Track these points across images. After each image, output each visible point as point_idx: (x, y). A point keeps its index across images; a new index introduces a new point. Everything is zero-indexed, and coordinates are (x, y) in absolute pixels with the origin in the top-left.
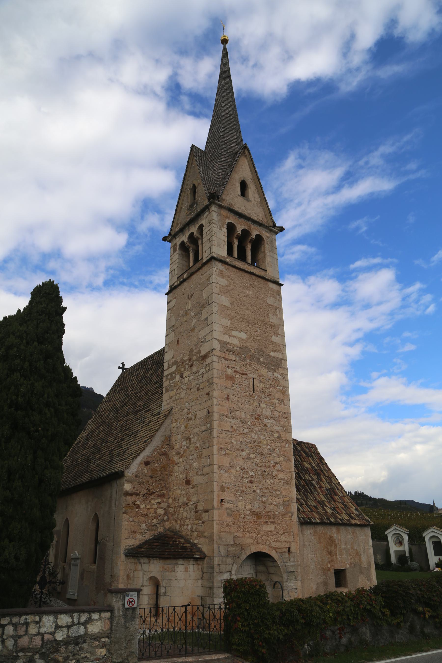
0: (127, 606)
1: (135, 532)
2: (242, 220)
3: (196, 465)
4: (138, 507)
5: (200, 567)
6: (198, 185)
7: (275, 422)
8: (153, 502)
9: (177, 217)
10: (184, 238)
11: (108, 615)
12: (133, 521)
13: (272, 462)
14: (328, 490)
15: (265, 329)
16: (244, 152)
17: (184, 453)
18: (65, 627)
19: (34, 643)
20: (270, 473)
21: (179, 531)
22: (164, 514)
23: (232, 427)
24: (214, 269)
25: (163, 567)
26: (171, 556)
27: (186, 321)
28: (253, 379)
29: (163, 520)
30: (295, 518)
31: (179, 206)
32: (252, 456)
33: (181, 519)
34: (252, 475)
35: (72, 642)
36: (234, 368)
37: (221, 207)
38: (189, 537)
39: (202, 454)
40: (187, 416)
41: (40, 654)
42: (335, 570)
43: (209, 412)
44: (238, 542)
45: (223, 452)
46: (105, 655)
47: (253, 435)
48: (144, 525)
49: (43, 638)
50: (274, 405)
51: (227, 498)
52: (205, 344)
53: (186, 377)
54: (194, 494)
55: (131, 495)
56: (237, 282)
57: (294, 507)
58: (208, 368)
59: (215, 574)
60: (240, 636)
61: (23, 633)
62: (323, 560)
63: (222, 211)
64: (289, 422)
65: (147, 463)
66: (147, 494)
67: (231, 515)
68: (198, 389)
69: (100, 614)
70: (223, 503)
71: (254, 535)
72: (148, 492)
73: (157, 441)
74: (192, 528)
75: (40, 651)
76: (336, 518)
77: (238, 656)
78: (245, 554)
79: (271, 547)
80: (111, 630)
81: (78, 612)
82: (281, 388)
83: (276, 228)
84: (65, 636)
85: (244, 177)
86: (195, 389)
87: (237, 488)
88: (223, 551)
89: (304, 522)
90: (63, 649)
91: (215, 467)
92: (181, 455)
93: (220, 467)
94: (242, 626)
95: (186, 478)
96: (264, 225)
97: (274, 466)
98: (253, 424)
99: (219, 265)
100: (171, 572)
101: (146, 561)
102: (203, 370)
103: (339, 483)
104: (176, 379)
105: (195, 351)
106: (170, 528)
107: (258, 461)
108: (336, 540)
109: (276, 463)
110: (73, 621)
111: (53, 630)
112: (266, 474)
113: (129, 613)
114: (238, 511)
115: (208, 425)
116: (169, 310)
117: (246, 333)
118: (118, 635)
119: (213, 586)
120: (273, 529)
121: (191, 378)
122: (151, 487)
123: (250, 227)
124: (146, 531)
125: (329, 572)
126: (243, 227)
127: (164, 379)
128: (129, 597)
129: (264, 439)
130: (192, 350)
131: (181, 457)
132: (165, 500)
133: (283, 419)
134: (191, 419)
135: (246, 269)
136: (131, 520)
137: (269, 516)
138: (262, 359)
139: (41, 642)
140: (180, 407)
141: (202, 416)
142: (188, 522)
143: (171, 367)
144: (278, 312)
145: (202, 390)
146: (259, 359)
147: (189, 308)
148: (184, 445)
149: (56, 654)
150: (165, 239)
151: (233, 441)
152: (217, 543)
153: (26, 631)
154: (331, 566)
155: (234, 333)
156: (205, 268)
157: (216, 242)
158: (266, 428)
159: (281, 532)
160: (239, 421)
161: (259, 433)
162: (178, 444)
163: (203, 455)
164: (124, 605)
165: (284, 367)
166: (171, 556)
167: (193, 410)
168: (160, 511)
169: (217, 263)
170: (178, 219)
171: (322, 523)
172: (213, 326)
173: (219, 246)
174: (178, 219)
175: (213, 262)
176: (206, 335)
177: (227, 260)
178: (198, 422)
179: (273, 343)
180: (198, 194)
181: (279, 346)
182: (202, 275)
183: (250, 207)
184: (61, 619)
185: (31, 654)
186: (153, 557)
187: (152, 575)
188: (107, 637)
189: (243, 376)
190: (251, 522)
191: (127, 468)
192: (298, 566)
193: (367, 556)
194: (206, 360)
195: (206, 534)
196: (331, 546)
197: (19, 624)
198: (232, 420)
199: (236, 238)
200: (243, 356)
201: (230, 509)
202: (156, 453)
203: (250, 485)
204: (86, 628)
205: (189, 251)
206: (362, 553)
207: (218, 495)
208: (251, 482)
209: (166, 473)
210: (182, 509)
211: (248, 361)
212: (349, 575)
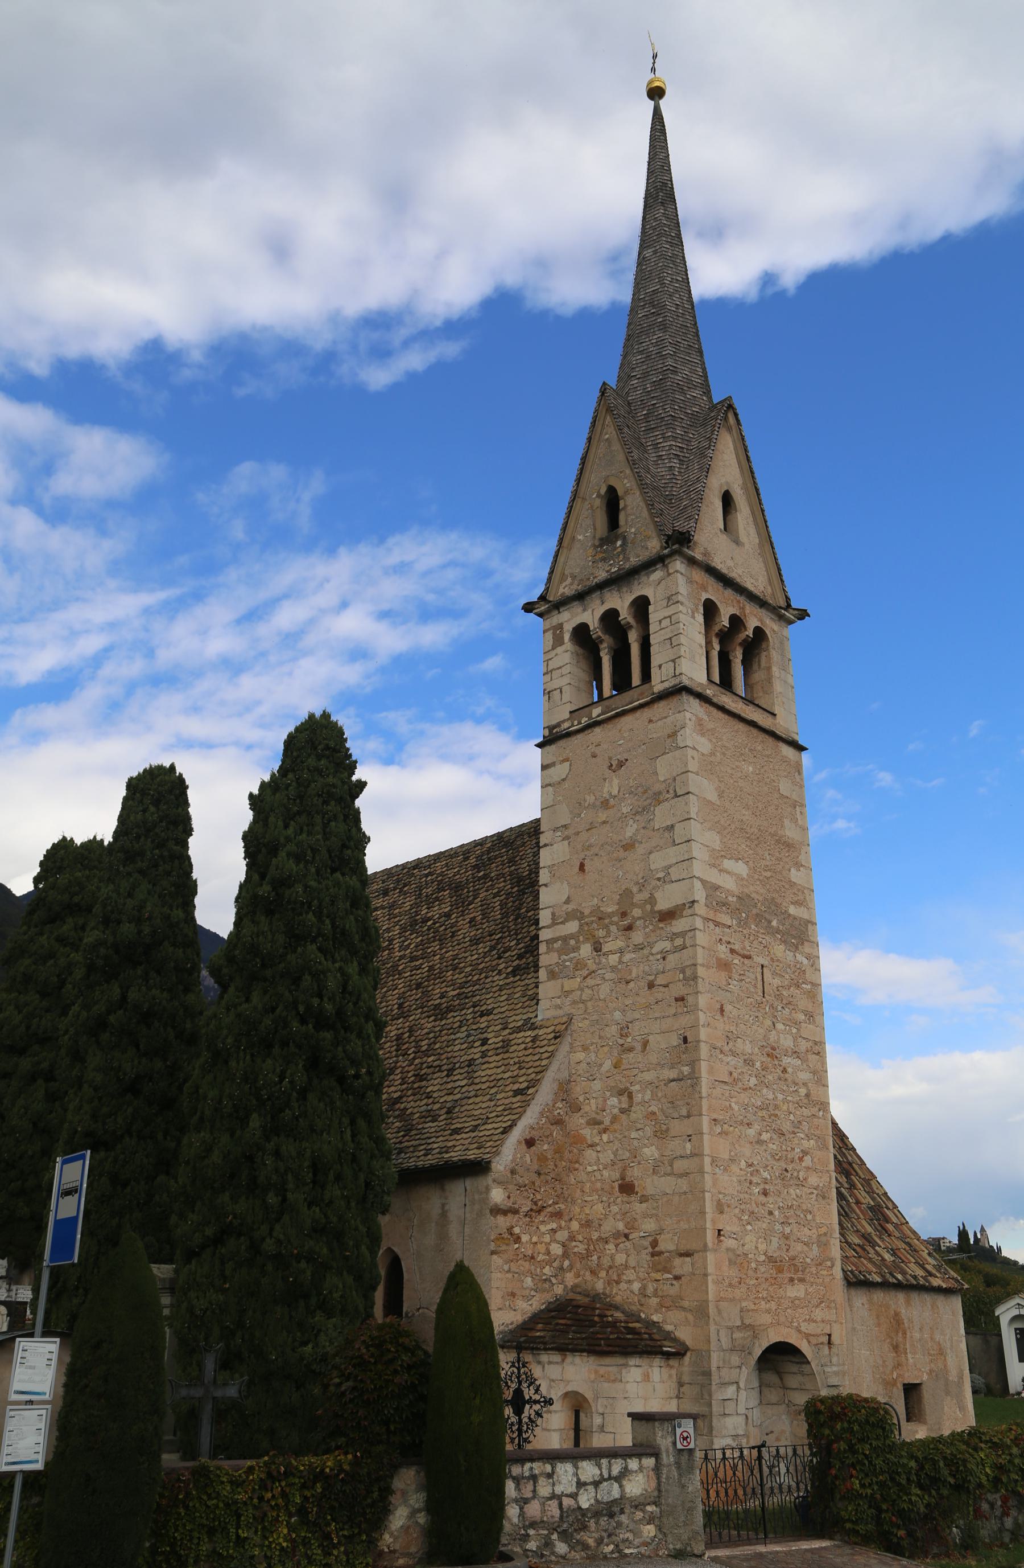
0: (679, 1446)
1: (513, 1295)
2: (729, 592)
3: (650, 1152)
4: (518, 1240)
5: (674, 1372)
6: (627, 492)
7: (800, 1062)
8: (543, 1228)
9: (561, 559)
10: (591, 615)
11: (649, 1462)
12: (509, 1271)
13: (797, 1150)
14: (871, 1208)
15: (777, 854)
16: (726, 419)
17: (612, 1123)
18: (591, 1483)
19: (549, 1513)
20: (795, 1174)
21: (604, 1294)
22: (563, 1255)
23: (731, 1074)
24: (688, 715)
25: (596, 1372)
26: (617, 1349)
27: (604, 822)
28: (762, 966)
29: (561, 1268)
30: (838, 1274)
31: (569, 531)
32: (765, 1136)
33: (610, 1267)
34: (766, 1179)
35: (605, 1512)
36: (729, 943)
37: (692, 561)
38: (633, 1308)
39: (668, 1130)
40: (621, 1041)
41: (559, 1533)
42: (904, 1385)
43: (685, 1040)
44: (747, 1322)
45: (718, 1130)
46: (655, 1536)
47: (765, 1091)
48: (529, 1279)
49: (560, 1505)
50: (797, 1023)
51: (728, 1228)
52: (667, 886)
53: (612, 952)
54: (645, 1216)
55: (505, 1212)
56: (727, 745)
57: (835, 1251)
58: (679, 942)
59: (714, 1387)
60: (859, 1504)
61: (530, 1495)
62: (884, 1362)
63: (694, 572)
64: (824, 1063)
65: (530, 1143)
66: (531, 1210)
67: (735, 1263)
68: (651, 985)
69: (640, 1460)
70: (722, 1238)
71: (773, 1305)
72: (534, 1207)
73: (545, 1094)
74: (644, 1288)
75: (558, 1526)
76: (904, 1273)
77: (856, 1544)
78: (760, 1345)
79: (800, 1331)
80: (659, 1491)
81: (607, 1457)
82: (809, 987)
83: (791, 611)
84: (593, 1501)
85: (727, 483)
86: (643, 984)
87: (743, 1207)
88: (725, 1342)
89: (856, 1282)
90: (592, 1524)
91: (707, 1160)
92: (602, 1126)
93: (714, 1161)
94: (863, 1486)
95: (623, 1178)
96: (770, 605)
97: (801, 1159)
98: (765, 1068)
99: (695, 703)
100: (614, 1381)
101: (556, 1357)
102: (666, 945)
103: (886, 1193)
104: (581, 952)
105: (639, 898)
106: (575, 1286)
107: (774, 1147)
108: (905, 1321)
109: (805, 1153)
110: (601, 1474)
111: (574, 1489)
112: (789, 1175)
113: (685, 1457)
114: (746, 1255)
115: (686, 1070)
116: (547, 785)
117: (747, 863)
118: (670, 1501)
119: (711, 1413)
120: (801, 1294)
121: (627, 957)
122: (539, 1197)
123: (743, 608)
124: (533, 1293)
125: (895, 1389)
126: (732, 611)
127: (543, 948)
128: (682, 1430)
129: (784, 1101)
130: (627, 894)
131: (605, 1131)
132: (563, 1223)
133: (814, 1056)
134: (631, 1050)
135: (743, 715)
136: (506, 1267)
137: (795, 1265)
138: (774, 923)
139: (559, 1512)
140: (595, 1017)
141: (663, 1046)
142: (630, 1274)
143: (562, 923)
144: (798, 813)
145: (662, 989)
146: (770, 922)
147: (615, 792)
148: (613, 1106)
149: (582, 1533)
150: (528, 608)
151: (733, 1104)
152: (716, 1324)
153: (534, 1491)
154: (899, 1376)
155: (728, 864)
156: (661, 707)
157: (683, 651)
158: (787, 1075)
159: (815, 1301)
160: (741, 1063)
161: (775, 1086)
162: (593, 1101)
163: (672, 1133)
164: (674, 1443)
165: (812, 939)
166: (617, 1349)
167: (636, 1029)
168: (557, 1250)
169: (691, 699)
170: (565, 563)
171: (885, 1285)
172: (691, 848)
173: (692, 659)
174: (565, 563)
175: (685, 697)
176: (671, 866)
177: (708, 692)
178: (653, 1058)
179: (792, 884)
180: (627, 516)
181: (803, 893)
182: (650, 721)
183: (743, 561)
184: (583, 1469)
185: (546, 1532)
186: (573, 1351)
187: (570, 1389)
188: (655, 1503)
189: (746, 961)
190: (766, 1279)
191: (497, 1153)
192: (844, 1374)
193: (957, 1357)
194: (674, 922)
195: (686, 1304)
196: (897, 1332)
197: (523, 1478)
198: (730, 1058)
199: (740, 644)
200: (744, 915)
201: (733, 1250)
202: (544, 1120)
203: (762, 1198)
204: (621, 1486)
205: (598, 651)
206: (949, 1351)
207: (713, 1221)
208: (765, 1193)
209: (564, 1164)
210: (611, 1246)
211: (753, 927)
212: (927, 1394)
